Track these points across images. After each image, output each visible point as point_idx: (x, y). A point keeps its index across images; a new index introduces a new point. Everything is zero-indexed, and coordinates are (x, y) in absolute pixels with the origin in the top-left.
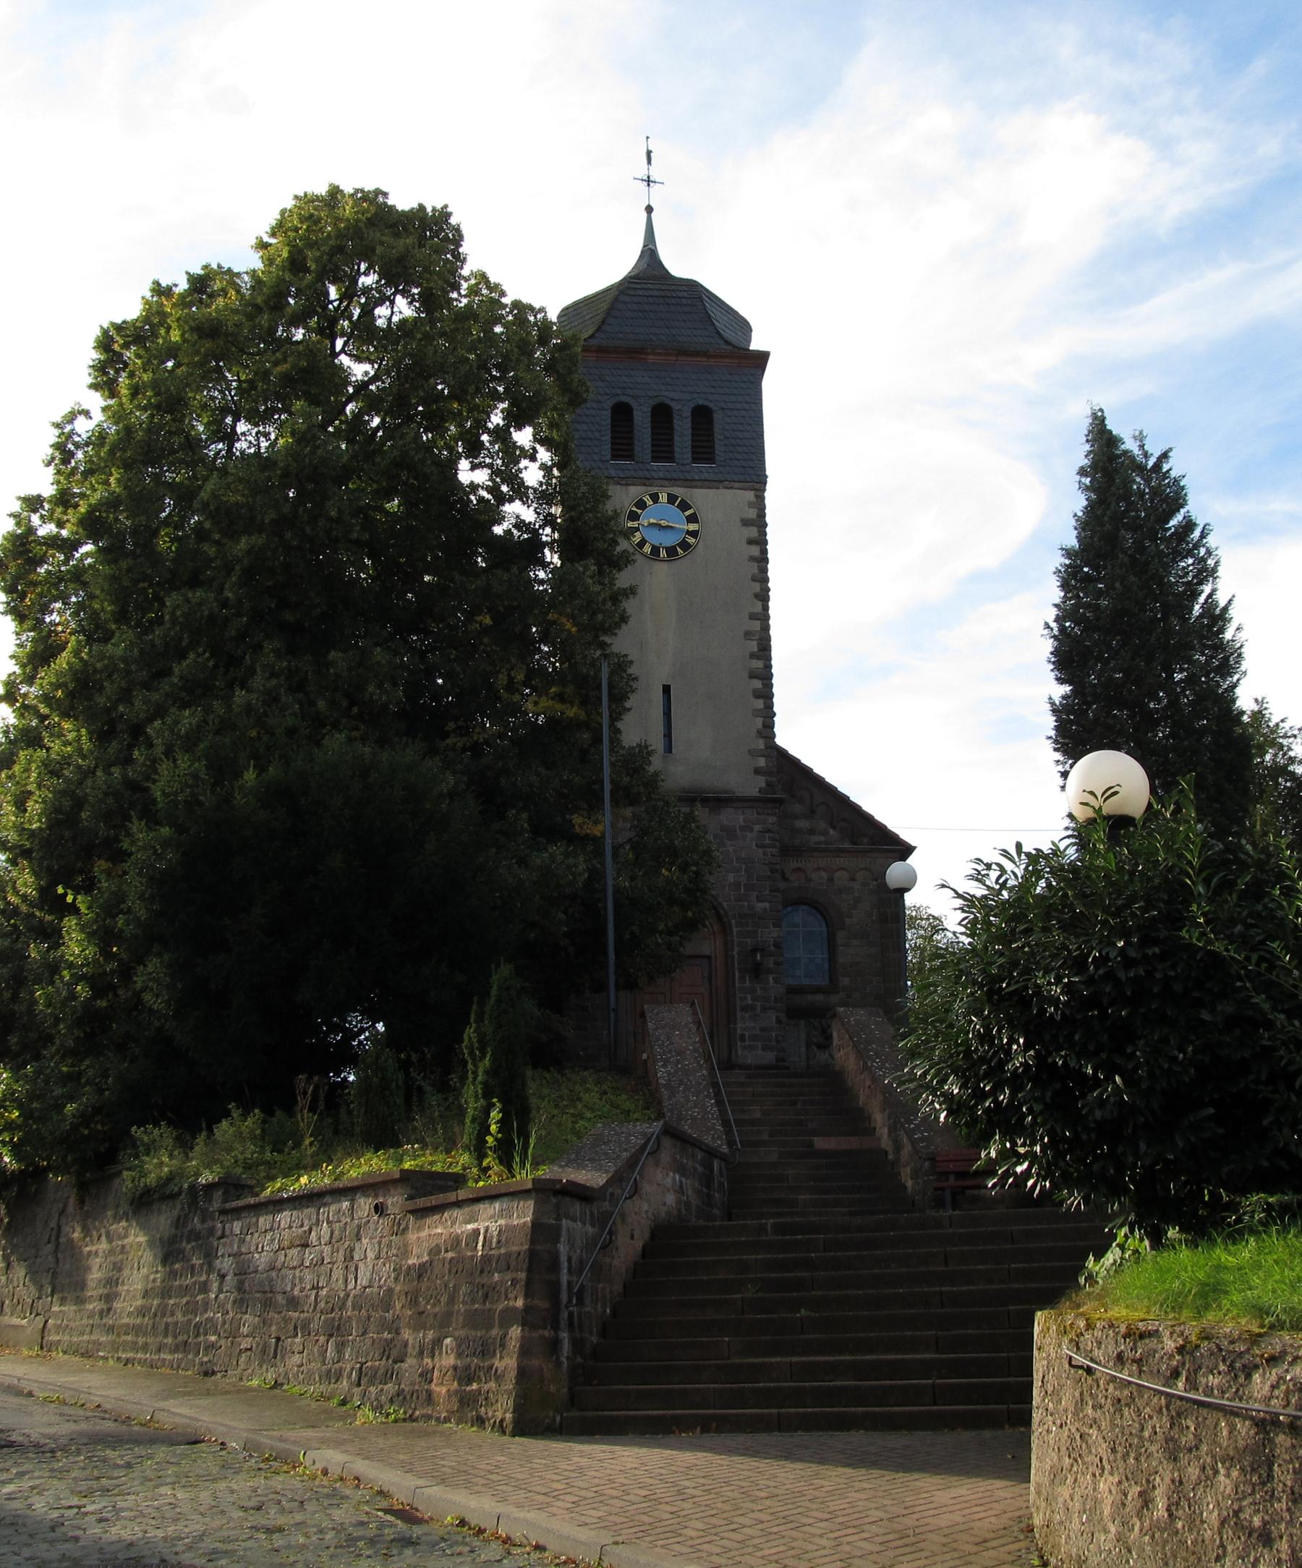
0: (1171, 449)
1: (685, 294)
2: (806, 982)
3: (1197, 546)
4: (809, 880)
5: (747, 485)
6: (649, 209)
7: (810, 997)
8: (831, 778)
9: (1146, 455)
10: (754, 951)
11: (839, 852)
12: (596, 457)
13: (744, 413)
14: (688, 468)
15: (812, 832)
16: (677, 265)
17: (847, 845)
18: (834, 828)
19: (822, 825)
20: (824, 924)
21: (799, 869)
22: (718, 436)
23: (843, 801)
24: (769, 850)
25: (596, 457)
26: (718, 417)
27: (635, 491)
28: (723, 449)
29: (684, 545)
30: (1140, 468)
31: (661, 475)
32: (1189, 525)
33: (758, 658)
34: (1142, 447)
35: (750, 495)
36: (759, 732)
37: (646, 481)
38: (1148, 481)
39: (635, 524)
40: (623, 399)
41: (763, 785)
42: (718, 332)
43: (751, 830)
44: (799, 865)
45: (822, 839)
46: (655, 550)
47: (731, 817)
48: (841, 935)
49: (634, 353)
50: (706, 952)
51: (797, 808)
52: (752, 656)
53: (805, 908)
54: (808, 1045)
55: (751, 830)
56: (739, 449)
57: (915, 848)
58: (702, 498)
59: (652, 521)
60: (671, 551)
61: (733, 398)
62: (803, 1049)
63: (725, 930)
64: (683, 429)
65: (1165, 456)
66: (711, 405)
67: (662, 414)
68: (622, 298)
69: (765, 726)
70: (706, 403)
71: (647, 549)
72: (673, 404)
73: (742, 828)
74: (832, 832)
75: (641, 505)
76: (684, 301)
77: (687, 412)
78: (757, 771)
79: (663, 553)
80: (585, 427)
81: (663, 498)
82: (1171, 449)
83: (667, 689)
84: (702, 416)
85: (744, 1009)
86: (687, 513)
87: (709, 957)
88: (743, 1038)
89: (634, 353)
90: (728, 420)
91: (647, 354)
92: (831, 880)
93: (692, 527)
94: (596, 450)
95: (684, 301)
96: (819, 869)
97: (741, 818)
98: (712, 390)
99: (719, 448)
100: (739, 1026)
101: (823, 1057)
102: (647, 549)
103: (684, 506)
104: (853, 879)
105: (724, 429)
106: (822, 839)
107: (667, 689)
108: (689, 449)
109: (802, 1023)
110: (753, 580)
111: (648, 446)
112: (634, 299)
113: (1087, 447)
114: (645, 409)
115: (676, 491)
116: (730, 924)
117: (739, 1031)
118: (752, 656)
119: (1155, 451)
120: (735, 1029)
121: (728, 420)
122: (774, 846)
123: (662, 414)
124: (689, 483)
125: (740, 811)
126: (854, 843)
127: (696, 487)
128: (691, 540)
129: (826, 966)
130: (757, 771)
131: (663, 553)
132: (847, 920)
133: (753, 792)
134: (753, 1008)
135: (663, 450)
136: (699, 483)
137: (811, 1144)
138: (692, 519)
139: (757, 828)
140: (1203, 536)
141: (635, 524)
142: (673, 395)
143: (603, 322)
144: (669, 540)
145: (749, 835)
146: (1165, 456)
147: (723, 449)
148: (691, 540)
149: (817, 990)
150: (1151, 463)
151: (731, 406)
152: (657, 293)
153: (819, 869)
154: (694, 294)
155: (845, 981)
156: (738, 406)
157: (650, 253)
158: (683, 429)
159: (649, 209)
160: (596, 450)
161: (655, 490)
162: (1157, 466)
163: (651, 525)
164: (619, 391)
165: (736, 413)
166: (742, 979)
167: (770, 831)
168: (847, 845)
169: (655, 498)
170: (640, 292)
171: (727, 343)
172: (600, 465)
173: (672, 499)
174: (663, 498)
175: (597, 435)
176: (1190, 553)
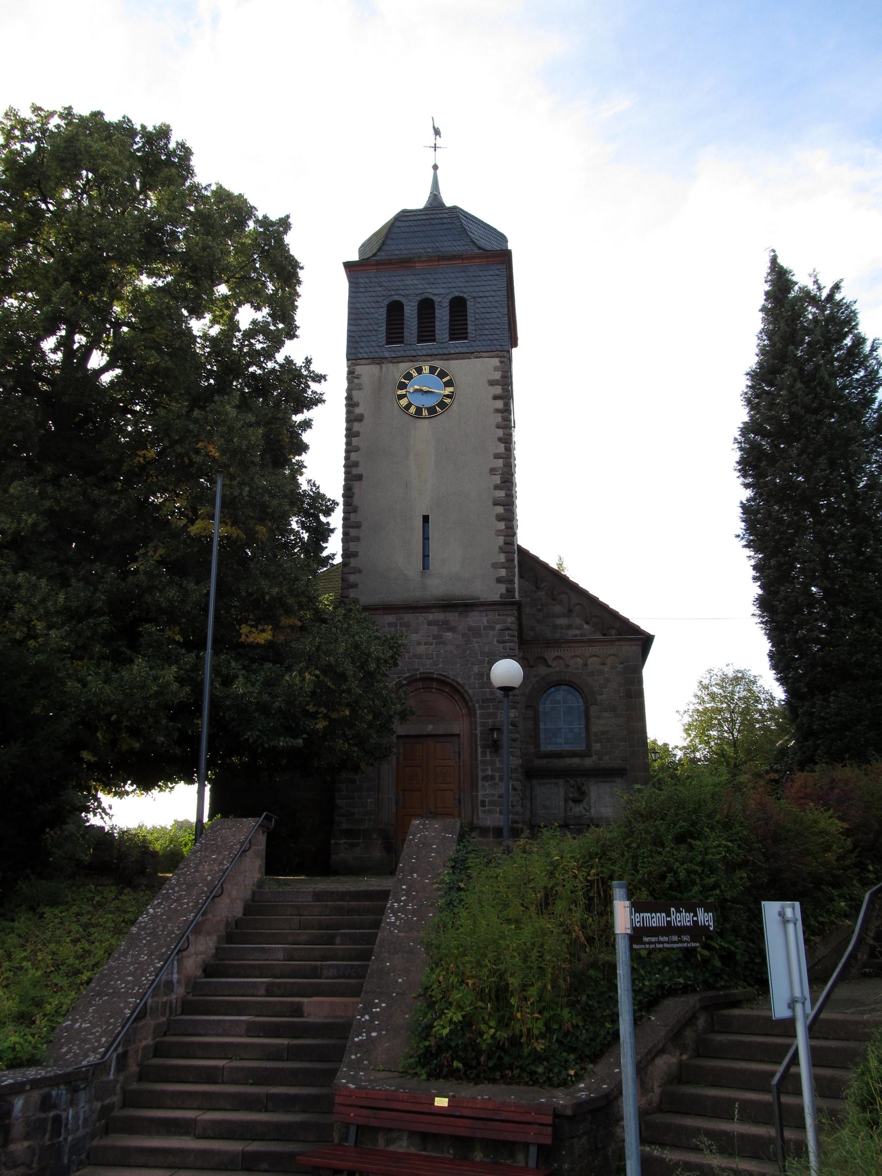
0: (842, 280)
1: (446, 216)
2: (567, 747)
3: (866, 357)
4: (568, 666)
5: (492, 354)
6: (435, 167)
7: (568, 761)
8: (583, 584)
9: (819, 289)
10: (492, 730)
11: (591, 642)
12: (374, 344)
13: (491, 299)
14: (445, 345)
15: (569, 627)
16: (448, 202)
17: (598, 636)
18: (587, 623)
19: (578, 621)
20: (581, 700)
21: (559, 657)
22: (470, 318)
23: (593, 601)
24: (508, 645)
25: (374, 344)
26: (470, 304)
27: (404, 367)
28: (474, 328)
29: (442, 405)
30: (814, 300)
31: (424, 352)
32: (859, 341)
33: (501, 489)
34: (816, 282)
35: (496, 362)
36: (500, 548)
37: (413, 358)
38: (822, 309)
39: (403, 392)
40: (396, 298)
41: (504, 591)
42: (473, 242)
43: (493, 629)
44: (559, 654)
45: (578, 632)
46: (419, 410)
47: (477, 619)
48: (593, 709)
49: (405, 263)
50: (456, 731)
51: (558, 609)
52: (496, 487)
53: (566, 687)
54: (566, 800)
55: (493, 629)
56: (487, 327)
57: (653, 636)
58: (455, 367)
59: (416, 387)
60: (432, 410)
61: (483, 289)
62: (562, 803)
63: (471, 713)
64: (442, 315)
65: (836, 287)
66: (465, 296)
67: (426, 307)
68: (397, 224)
69: (506, 543)
70: (461, 295)
71: (412, 410)
72: (435, 298)
73: (485, 628)
74: (586, 626)
75: (409, 376)
76: (445, 221)
77: (446, 303)
78: (499, 580)
79: (425, 413)
80: (366, 322)
81: (426, 370)
82: (842, 280)
83: (426, 519)
84: (458, 306)
85: (485, 778)
86: (447, 378)
87: (458, 735)
88: (483, 803)
89: (405, 263)
90: (478, 305)
91: (415, 262)
92: (585, 665)
93: (448, 391)
94: (374, 338)
95: (445, 221)
96: (576, 656)
97: (485, 619)
98: (466, 284)
99: (471, 328)
100: (481, 793)
101: (578, 809)
102: (412, 410)
103: (442, 375)
104: (604, 664)
105: (475, 313)
106: (578, 632)
107: (426, 519)
108: (447, 330)
109: (561, 782)
110: (498, 427)
111: (415, 331)
112: (407, 224)
113: (767, 287)
114: (413, 304)
115: (439, 364)
116: (474, 706)
117: (480, 798)
118: (496, 487)
119: (827, 285)
120: (477, 796)
121: (478, 305)
122: (512, 641)
123: (426, 307)
124: (447, 356)
125: (484, 614)
126: (604, 635)
127: (453, 359)
128: (448, 401)
129: (583, 735)
130: (499, 580)
131: (425, 413)
132: (599, 697)
133: (496, 598)
134: (492, 778)
135: (426, 333)
136: (455, 356)
137: (297, 1010)
138: (449, 384)
139: (498, 627)
140: (874, 349)
141: (403, 392)
142: (436, 292)
143: (383, 244)
144: (431, 401)
145: (491, 633)
146: (836, 287)
147: (474, 328)
148: (448, 401)
149: (575, 754)
150: (824, 294)
151: (481, 294)
152: (424, 217)
153: (576, 656)
154: (456, 212)
155: (597, 746)
156: (487, 294)
157: (435, 197)
158: (442, 315)
159: (435, 167)
160: (374, 338)
161: (418, 365)
162: (830, 297)
163: (416, 391)
164: (393, 293)
165: (485, 300)
166: (484, 754)
167: (508, 629)
168: (598, 636)
169: (419, 370)
170: (411, 218)
171: (480, 248)
172: (377, 349)
173: (433, 370)
174: (426, 370)
175: (376, 327)
176: (862, 364)
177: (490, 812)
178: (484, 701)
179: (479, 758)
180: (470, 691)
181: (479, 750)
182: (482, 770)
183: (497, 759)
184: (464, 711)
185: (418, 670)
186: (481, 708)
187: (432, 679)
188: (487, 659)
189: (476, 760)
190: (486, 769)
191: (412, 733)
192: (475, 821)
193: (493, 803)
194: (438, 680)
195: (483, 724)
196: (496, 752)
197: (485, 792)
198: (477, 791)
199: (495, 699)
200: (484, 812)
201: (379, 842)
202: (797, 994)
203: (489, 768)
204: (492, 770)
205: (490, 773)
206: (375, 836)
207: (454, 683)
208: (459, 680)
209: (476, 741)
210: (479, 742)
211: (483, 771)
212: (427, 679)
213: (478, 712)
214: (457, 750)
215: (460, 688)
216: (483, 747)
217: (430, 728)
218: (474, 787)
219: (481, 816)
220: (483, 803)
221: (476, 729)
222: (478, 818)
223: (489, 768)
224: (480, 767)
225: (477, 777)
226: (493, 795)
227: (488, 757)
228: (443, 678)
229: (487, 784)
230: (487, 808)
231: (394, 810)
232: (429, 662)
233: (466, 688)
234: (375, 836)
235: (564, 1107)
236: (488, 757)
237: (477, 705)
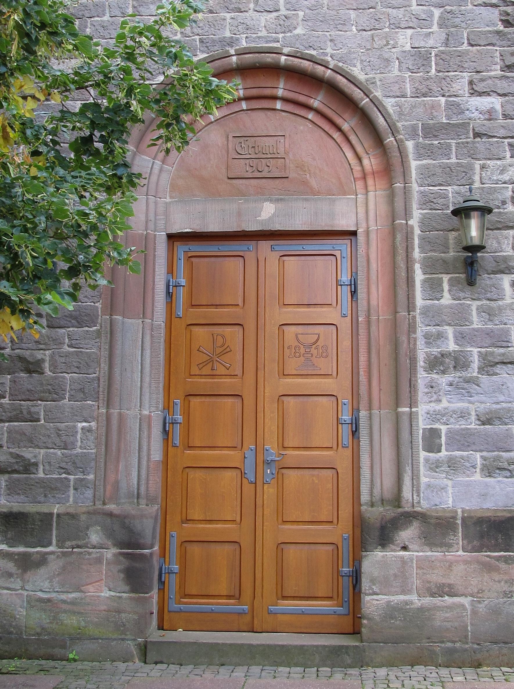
10: (462, 213)
50: (345, 223)
63: (390, 167)
85: (436, 363)
87: (354, 233)
88: (432, 440)
100: (423, 409)
117: (422, 424)
120: (412, 417)
134: (460, 362)
166: (433, 288)
177: (453, 465)
178: (431, 131)
179: (420, 302)
180: (389, 104)
181: (419, 276)
182: (427, 336)
183: (475, 305)
184: (370, 162)
185: (231, 42)
186: (423, 152)
187: (275, 70)
188: (437, 13)
189: (410, 306)
190: (440, 336)
191: (214, 226)
192: (407, 493)
193: (462, 440)
194: (292, 73)
195: (427, 201)
196: (471, 282)
197: (434, 404)
198: (413, 403)
199: (464, 125)
200: (434, 467)
201: (110, 553)
202: (167, 575)
203: (450, 331)
204: (460, 338)
205: (452, 346)
206: (95, 537)
207: (341, 81)
208: (357, 72)
209: (409, 250)
210: (417, 254)
211: (431, 339)
212: (259, 70)
213: (414, 164)
214: (345, 278)
215: (357, 94)
216: (430, 266)
217: (267, 214)
218: (402, 390)
219: (424, 480)
220: (432, 440)
221: (407, 215)
222: (416, 487)
223: (450, 331)
224: (421, 329)
225: (413, 360)
226: (463, 415)
227: (447, 300)
228: (305, 64)
229: (443, 380)
230: (444, 453)
231: (157, 455)
232: (264, 19)
233: (378, 94)
234: (95, 537)
235: (97, 532)
236: (447, 300)
237: (410, 145)
